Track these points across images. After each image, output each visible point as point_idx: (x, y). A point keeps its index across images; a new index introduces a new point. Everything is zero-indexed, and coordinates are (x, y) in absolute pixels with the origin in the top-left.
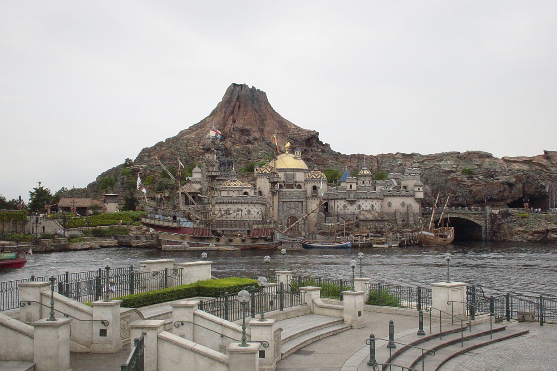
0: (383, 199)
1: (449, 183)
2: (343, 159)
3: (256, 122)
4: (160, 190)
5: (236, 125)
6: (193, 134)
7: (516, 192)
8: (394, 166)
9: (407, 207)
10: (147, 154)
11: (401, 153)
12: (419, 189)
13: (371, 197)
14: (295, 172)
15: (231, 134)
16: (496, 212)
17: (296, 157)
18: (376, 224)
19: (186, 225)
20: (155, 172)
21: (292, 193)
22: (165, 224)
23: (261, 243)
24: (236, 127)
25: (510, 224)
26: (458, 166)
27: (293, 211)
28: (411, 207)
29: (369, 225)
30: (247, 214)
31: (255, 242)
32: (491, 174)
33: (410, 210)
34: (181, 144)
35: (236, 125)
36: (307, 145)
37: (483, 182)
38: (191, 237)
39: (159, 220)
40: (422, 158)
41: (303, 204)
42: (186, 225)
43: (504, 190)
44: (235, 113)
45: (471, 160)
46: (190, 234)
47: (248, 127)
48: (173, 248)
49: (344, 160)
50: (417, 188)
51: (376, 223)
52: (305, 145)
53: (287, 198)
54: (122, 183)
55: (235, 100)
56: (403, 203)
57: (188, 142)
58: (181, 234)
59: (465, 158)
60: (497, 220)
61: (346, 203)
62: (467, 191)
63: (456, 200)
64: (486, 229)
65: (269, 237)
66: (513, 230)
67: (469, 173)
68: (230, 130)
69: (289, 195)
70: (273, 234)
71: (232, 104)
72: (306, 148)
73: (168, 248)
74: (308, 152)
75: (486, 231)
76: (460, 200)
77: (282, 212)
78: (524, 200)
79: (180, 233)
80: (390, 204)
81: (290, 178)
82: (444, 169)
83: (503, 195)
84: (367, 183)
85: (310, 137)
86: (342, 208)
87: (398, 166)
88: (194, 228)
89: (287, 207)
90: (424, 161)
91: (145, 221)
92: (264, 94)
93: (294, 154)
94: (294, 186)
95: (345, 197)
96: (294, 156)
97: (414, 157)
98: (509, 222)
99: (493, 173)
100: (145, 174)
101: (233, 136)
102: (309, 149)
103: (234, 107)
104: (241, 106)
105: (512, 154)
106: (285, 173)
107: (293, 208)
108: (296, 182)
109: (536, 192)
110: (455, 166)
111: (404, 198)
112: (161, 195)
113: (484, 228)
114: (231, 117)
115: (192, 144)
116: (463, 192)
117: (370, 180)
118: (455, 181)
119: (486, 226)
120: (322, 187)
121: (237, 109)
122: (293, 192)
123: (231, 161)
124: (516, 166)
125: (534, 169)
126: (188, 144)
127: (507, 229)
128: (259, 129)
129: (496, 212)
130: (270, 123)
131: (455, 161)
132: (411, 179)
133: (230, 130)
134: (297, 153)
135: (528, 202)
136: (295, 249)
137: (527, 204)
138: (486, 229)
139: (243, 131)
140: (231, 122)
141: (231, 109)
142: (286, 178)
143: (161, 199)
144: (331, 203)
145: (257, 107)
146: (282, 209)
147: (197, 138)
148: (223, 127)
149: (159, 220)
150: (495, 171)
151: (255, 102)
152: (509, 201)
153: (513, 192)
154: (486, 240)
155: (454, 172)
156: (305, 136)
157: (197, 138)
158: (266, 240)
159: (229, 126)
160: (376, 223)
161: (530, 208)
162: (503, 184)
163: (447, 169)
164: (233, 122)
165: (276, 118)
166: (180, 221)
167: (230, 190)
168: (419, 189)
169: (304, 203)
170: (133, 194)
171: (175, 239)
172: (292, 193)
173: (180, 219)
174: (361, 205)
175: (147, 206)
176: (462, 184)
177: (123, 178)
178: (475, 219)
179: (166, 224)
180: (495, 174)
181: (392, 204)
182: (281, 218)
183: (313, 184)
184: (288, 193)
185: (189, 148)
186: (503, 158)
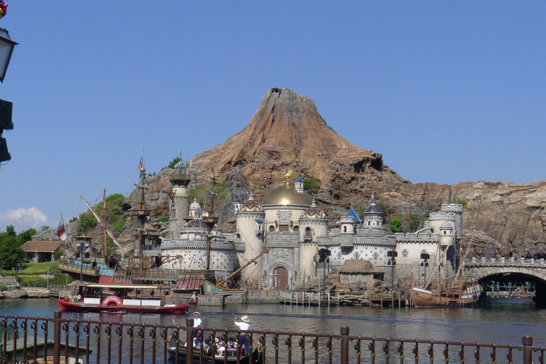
1: (531, 223)
3: (292, 141)
5: (265, 145)
12: (445, 233)
19: (106, 272)
22: (91, 272)
24: (263, 149)
27: (281, 260)
30: (373, 258)
42: (106, 272)
44: (268, 128)
47: (279, 149)
53: (273, 243)
55: (270, 110)
69: (276, 239)
81: (284, 218)
86: (336, 257)
87: (474, 200)
91: (66, 269)
103: (267, 122)
104: (275, 119)
106: (278, 210)
117: (378, 220)
120: (319, 230)
134: (297, 184)
136: (213, 304)
139: (272, 154)
142: (279, 217)
145: (296, 121)
156: (354, 159)
157: (211, 164)
168: (445, 233)
169: (296, 250)
174: (360, 253)
181: (408, 252)
182: (265, 268)
183: (307, 226)
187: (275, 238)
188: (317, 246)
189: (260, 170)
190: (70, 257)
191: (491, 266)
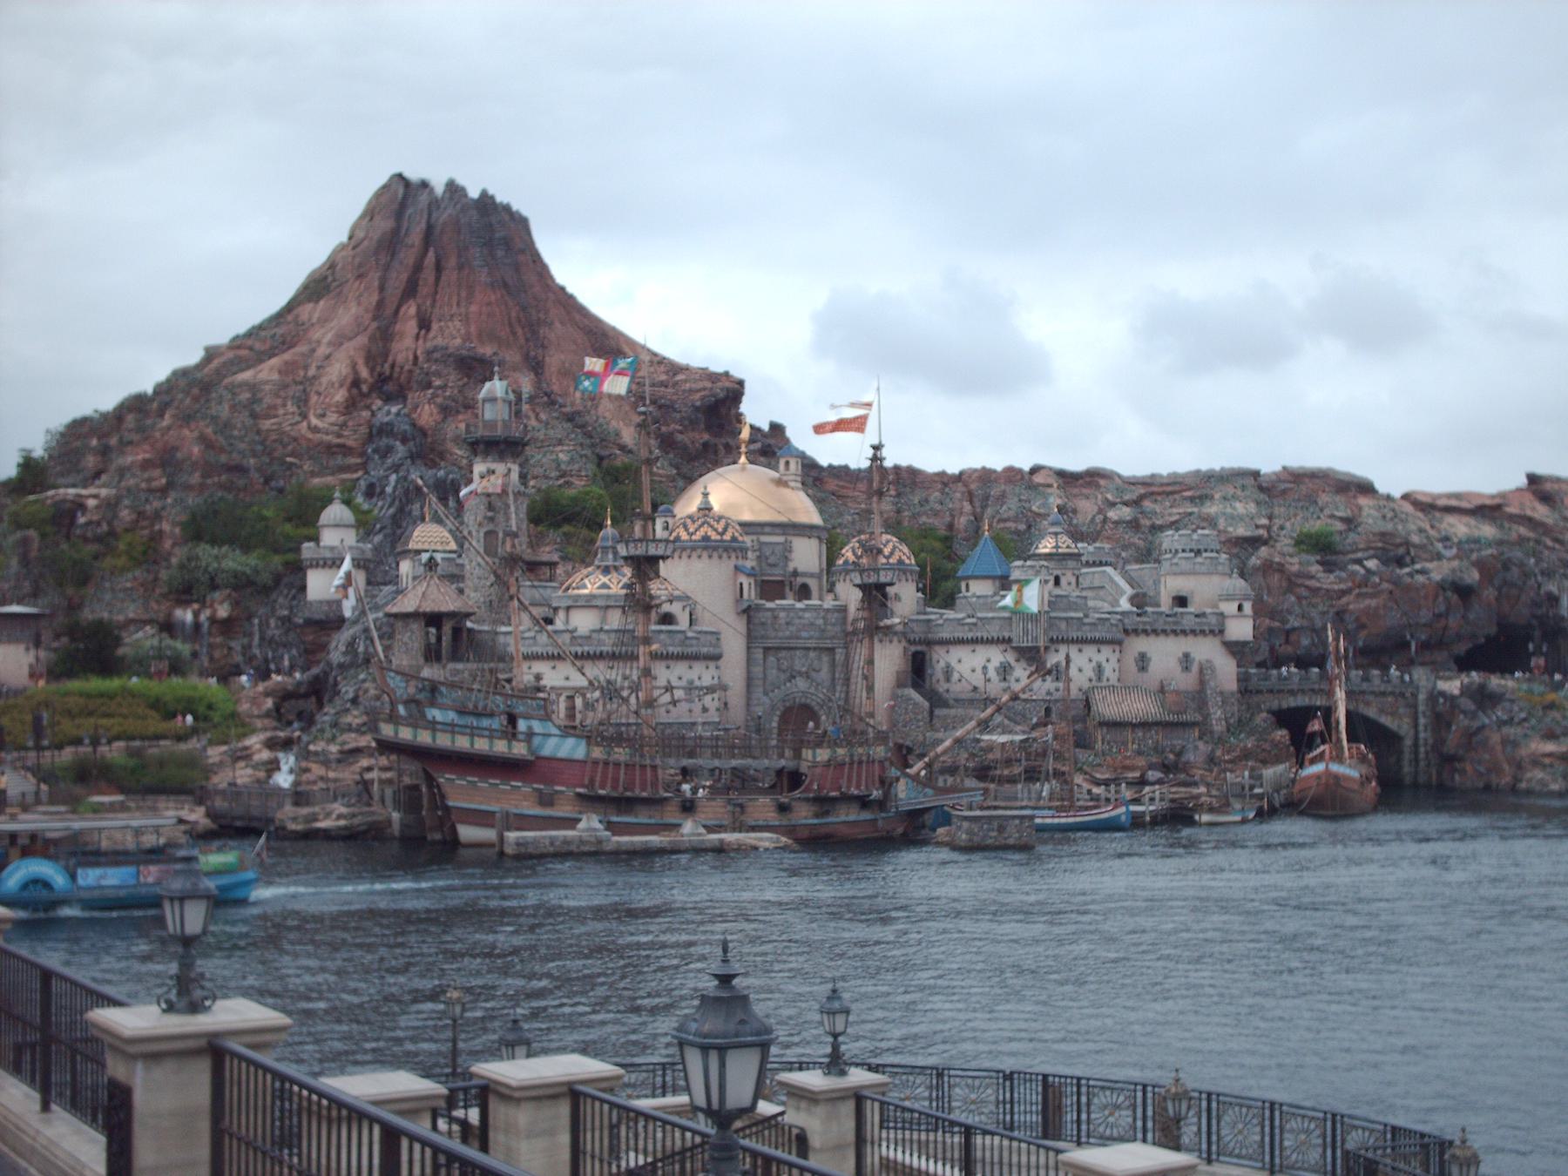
0: (1120, 643)
2: (841, 483)
3: (514, 333)
4: (185, 593)
5: (436, 338)
6: (271, 369)
7: (1480, 621)
8: (1039, 515)
9: (1201, 671)
10: (94, 442)
11: (1050, 469)
12: (1240, 608)
13: (1097, 635)
14: (789, 538)
15: (427, 374)
16: (1453, 686)
17: (785, 478)
18: (1155, 736)
19: (558, 747)
20: (157, 516)
21: (800, 618)
22: (477, 746)
23: (847, 815)
25: (1506, 730)
26: (1270, 518)
28: (1213, 669)
29: (1133, 741)
31: (826, 813)
32: (1395, 553)
33: (1212, 684)
34: (233, 408)
35: (436, 338)
36: (708, 428)
37: (1381, 579)
38: (579, 795)
39: (452, 728)
40: (1133, 488)
41: (834, 660)
42: (558, 747)
43: (1448, 610)
44: (424, 290)
45: (1311, 499)
46: (576, 786)
48: (552, 844)
49: (843, 487)
50: (1235, 605)
51: (1157, 734)
52: (702, 426)
53: (780, 634)
54: (25, 561)
56: (1186, 656)
57: (255, 400)
58: (542, 787)
59: (1284, 492)
60: (1462, 717)
61: (1010, 657)
62: (1327, 612)
63: (1287, 642)
64: (1416, 745)
65: (876, 794)
66: (1523, 752)
67: (1322, 547)
68: (416, 358)
69: (788, 624)
70: (886, 784)
71: (408, 257)
72: (706, 437)
73: (536, 841)
74: (716, 452)
75: (1416, 753)
76: (1305, 642)
77: (761, 689)
78: (1531, 647)
79: (536, 782)
80: (1143, 662)
81: (772, 560)
82: (1231, 529)
83: (1445, 628)
84: (1069, 584)
85: (722, 395)
88: (596, 763)
89: (779, 669)
90: (1142, 497)
92: (522, 223)
93: (775, 468)
94: (787, 589)
95: (1006, 635)
96: (776, 475)
97: (1102, 482)
98: (1505, 723)
99: (1401, 551)
100: (110, 524)
101: (438, 383)
102: (716, 440)
103: (418, 267)
105: (1437, 480)
106: (755, 537)
107: (800, 673)
108: (795, 573)
109: (1534, 616)
110: (1264, 521)
111: (1190, 639)
112: (196, 614)
113: (1408, 742)
114: (411, 309)
115: (275, 407)
116: (1314, 613)
118: (1277, 576)
119: (1416, 738)
121: (428, 275)
122: (801, 614)
123: (453, 481)
124: (1460, 527)
125: (1514, 536)
126: (257, 408)
127: (1499, 748)
128: (526, 357)
129: (1453, 686)
130: (557, 332)
131: (1258, 503)
132: (1204, 569)
133: (416, 358)
134: (787, 463)
135: (1542, 654)
136: (1011, 841)
137: (1542, 661)
138: (1416, 745)
140: (411, 327)
141: (404, 276)
143: (197, 626)
144: (942, 658)
146: (761, 676)
147: (286, 386)
148: (380, 345)
149: (452, 728)
150: (1407, 544)
151: (500, 253)
152: (1461, 648)
153: (1472, 616)
154: (1415, 785)
155: (1265, 543)
158: (864, 802)
159: (408, 342)
160: (1157, 734)
161: (1552, 676)
162: (1444, 589)
163: (1241, 531)
164: (420, 328)
165: (578, 317)
166: (530, 735)
167: (608, 607)
169: (840, 655)
170: (80, 606)
171: (516, 806)
172: (800, 618)
173: (530, 728)
175: (392, 674)
176: (1307, 587)
177: (25, 542)
178: (1382, 711)
179: (481, 745)
180: (1408, 553)
181: (1150, 659)
182: (759, 711)
184: (782, 615)
185: (267, 424)
186: (1406, 497)
187: (783, 621)
188: (904, 643)
189: (462, 410)
190: (405, 697)
191: (1271, 691)
